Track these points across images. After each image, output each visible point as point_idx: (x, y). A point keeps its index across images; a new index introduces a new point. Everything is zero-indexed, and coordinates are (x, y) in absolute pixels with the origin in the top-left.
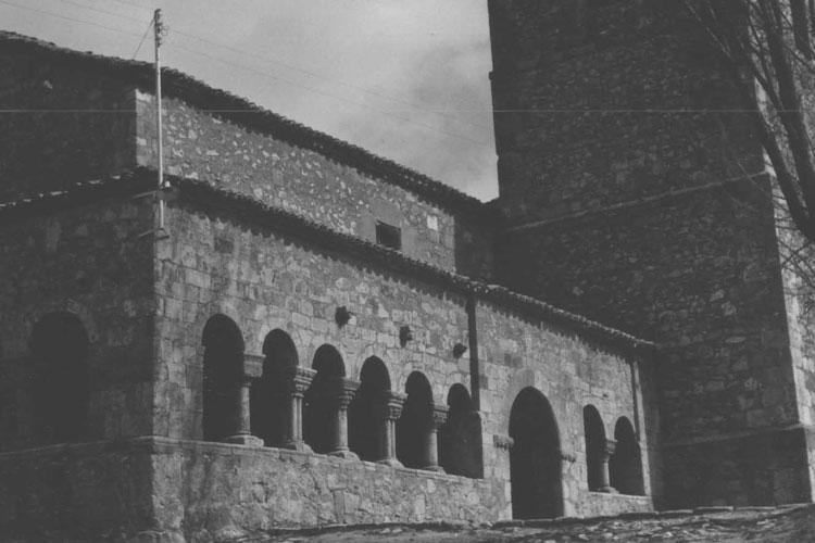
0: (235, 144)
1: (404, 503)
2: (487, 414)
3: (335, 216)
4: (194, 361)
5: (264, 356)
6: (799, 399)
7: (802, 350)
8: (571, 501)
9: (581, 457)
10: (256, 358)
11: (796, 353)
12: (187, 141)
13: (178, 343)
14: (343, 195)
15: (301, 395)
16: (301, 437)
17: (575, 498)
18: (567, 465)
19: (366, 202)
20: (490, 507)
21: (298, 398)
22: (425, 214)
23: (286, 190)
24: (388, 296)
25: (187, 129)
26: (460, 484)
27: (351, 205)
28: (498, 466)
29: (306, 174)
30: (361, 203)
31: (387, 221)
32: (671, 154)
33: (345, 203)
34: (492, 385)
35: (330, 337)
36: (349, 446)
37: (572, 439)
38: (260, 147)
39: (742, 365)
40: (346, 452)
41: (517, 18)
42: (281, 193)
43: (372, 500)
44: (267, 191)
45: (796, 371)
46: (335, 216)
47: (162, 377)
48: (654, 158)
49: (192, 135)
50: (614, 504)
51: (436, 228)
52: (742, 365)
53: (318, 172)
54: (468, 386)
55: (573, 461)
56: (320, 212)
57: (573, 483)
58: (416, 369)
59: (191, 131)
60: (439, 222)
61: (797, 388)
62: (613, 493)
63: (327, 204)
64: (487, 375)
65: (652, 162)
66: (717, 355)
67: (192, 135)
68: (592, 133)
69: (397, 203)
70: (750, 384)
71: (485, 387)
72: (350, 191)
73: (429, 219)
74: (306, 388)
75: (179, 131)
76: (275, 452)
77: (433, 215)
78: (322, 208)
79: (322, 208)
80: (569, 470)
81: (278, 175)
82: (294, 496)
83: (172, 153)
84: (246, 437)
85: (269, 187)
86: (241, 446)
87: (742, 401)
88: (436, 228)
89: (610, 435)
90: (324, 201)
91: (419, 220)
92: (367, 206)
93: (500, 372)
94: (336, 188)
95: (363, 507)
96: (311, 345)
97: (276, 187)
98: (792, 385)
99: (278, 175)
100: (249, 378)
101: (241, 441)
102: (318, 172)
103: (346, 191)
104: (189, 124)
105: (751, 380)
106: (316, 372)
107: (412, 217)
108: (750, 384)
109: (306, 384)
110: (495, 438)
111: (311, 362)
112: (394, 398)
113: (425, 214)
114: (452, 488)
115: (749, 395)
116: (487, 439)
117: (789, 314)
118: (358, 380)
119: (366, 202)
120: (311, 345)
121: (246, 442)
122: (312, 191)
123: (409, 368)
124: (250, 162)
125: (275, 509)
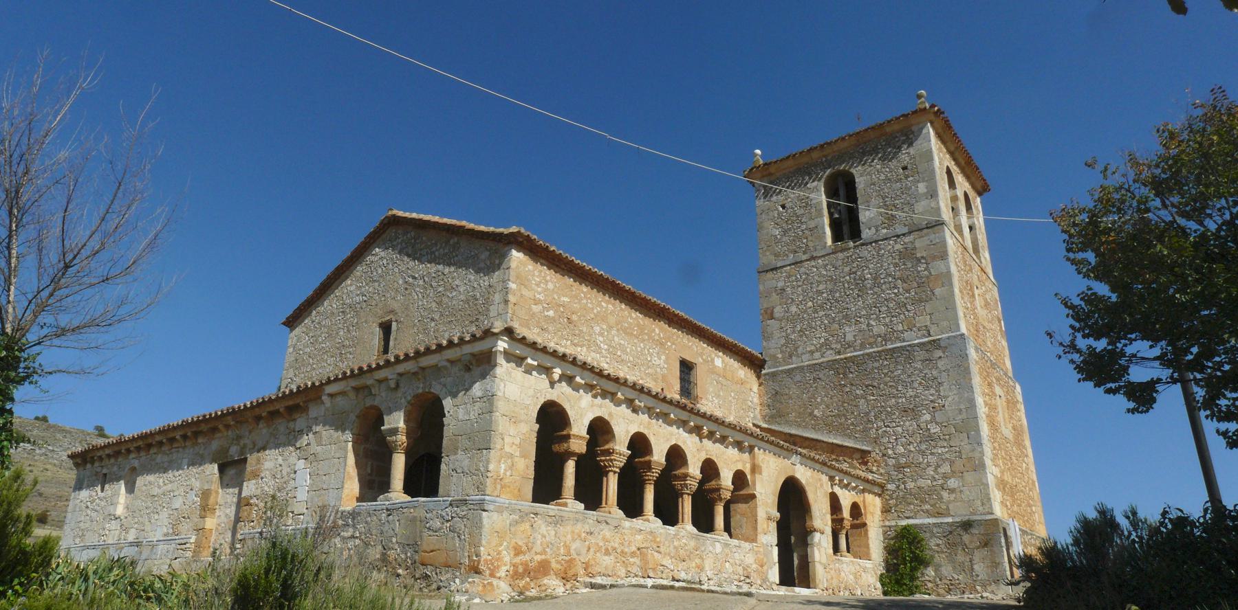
0: (582, 295)
1: (698, 561)
2: (761, 494)
3: (651, 350)
4: (527, 436)
5: (588, 436)
6: (992, 496)
7: (991, 460)
8: (820, 562)
9: (828, 530)
10: (581, 438)
11: (988, 462)
12: (546, 290)
13: (514, 420)
14: (657, 338)
15: (618, 470)
16: (616, 504)
17: (824, 560)
18: (817, 536)
19: (673, 344)
20: (762, 566)
21: (615, 472)
22: (713, 356)
23: (618, 330)
24: (610, 588)
25: (547, 281)
26: (740, 547)
27: (662, 344)
28: (769, 538)
29: (631, 321)
30: (669, 344)
31: (688, 358)
32: (887, 320)
33: (658, 343)
34: (765, 473)
35: (642, 426)
36: (654, 513)
37: (821, 517)
38: (600, 300)
39: (946, 468)
40: (652, 517)
41: (778, 233)
42: (614, 332)
43: (671, 558)
44: (603, 329)
45: (989, 475)
46: (651, 350)
47: (498, 447)
48: (874, 323)
49: (550, 286)
50: (851, 566)
51: (720, 365)
52: (946, 468)
53: (640, 320)
54: (748, 472)
55: (822, 533)
56: (640, 347)
57: (822, 550)
58: (708, 457)
59: (550, 283)
60: (723, 361)
61: (991, 488)
62: (848, 558)
63: (645, 342)
64: (761, 464)
65: (872, 326)
66: (926, 460)
67: (550, 286)
68: (828, 307)
69: (694, 347)
70: (953, 483)
71: (760, 474)
72: (662, 335)
73: (716, 359)
74: (623, 464)
75: (540, 282)
76: (593, 515)
77: (718, 357)
78: (642, 345)
79: (642, 345)
80: (820, 540)
81: (612, 320)
82: (607, 553)
83: (535, 296)
84: (568, 501)
85: (605, 327)
86: (565, 508)
87: (945, 494)
88: (720, 365)
89: (846, 513)
90: (643, 340)
91: (709, 359)
92: (674, 346)
93: (771, 463)
94: (652, 332)
95: (664, 563)
96: (627, 432)
97: (611, 328)
98: (987, 485)
99: (612, 320)
100: (573, 454)
101: (565, 505)
102: (640, 320)
103: (659, 334)
104: (548, 278)
105: (952, 480)
106: (630, 452)
107: (704, 357)
108: (953, 483)
109: (621, 462)
110: (767, 513)
111: (627, 445)
112: (691, 477)
113: (713, 356)
114: (734, 550)
115: (952, 491)
116: (761, 514)
117: (982, 433)
118: (663, 461)
119: (673, 344)
120: (627, 432)
121: (569, 505)
122: (635, 332)
123: (703, 457)
124: (593, 309)
125: (592, 562)
